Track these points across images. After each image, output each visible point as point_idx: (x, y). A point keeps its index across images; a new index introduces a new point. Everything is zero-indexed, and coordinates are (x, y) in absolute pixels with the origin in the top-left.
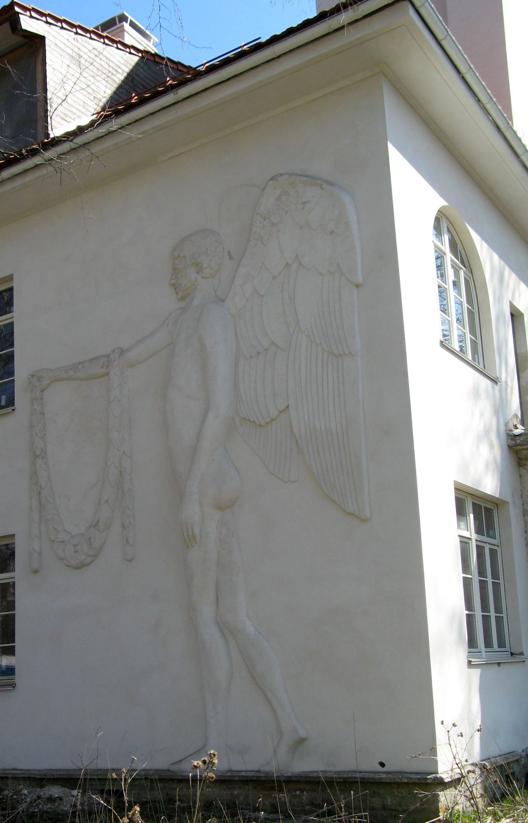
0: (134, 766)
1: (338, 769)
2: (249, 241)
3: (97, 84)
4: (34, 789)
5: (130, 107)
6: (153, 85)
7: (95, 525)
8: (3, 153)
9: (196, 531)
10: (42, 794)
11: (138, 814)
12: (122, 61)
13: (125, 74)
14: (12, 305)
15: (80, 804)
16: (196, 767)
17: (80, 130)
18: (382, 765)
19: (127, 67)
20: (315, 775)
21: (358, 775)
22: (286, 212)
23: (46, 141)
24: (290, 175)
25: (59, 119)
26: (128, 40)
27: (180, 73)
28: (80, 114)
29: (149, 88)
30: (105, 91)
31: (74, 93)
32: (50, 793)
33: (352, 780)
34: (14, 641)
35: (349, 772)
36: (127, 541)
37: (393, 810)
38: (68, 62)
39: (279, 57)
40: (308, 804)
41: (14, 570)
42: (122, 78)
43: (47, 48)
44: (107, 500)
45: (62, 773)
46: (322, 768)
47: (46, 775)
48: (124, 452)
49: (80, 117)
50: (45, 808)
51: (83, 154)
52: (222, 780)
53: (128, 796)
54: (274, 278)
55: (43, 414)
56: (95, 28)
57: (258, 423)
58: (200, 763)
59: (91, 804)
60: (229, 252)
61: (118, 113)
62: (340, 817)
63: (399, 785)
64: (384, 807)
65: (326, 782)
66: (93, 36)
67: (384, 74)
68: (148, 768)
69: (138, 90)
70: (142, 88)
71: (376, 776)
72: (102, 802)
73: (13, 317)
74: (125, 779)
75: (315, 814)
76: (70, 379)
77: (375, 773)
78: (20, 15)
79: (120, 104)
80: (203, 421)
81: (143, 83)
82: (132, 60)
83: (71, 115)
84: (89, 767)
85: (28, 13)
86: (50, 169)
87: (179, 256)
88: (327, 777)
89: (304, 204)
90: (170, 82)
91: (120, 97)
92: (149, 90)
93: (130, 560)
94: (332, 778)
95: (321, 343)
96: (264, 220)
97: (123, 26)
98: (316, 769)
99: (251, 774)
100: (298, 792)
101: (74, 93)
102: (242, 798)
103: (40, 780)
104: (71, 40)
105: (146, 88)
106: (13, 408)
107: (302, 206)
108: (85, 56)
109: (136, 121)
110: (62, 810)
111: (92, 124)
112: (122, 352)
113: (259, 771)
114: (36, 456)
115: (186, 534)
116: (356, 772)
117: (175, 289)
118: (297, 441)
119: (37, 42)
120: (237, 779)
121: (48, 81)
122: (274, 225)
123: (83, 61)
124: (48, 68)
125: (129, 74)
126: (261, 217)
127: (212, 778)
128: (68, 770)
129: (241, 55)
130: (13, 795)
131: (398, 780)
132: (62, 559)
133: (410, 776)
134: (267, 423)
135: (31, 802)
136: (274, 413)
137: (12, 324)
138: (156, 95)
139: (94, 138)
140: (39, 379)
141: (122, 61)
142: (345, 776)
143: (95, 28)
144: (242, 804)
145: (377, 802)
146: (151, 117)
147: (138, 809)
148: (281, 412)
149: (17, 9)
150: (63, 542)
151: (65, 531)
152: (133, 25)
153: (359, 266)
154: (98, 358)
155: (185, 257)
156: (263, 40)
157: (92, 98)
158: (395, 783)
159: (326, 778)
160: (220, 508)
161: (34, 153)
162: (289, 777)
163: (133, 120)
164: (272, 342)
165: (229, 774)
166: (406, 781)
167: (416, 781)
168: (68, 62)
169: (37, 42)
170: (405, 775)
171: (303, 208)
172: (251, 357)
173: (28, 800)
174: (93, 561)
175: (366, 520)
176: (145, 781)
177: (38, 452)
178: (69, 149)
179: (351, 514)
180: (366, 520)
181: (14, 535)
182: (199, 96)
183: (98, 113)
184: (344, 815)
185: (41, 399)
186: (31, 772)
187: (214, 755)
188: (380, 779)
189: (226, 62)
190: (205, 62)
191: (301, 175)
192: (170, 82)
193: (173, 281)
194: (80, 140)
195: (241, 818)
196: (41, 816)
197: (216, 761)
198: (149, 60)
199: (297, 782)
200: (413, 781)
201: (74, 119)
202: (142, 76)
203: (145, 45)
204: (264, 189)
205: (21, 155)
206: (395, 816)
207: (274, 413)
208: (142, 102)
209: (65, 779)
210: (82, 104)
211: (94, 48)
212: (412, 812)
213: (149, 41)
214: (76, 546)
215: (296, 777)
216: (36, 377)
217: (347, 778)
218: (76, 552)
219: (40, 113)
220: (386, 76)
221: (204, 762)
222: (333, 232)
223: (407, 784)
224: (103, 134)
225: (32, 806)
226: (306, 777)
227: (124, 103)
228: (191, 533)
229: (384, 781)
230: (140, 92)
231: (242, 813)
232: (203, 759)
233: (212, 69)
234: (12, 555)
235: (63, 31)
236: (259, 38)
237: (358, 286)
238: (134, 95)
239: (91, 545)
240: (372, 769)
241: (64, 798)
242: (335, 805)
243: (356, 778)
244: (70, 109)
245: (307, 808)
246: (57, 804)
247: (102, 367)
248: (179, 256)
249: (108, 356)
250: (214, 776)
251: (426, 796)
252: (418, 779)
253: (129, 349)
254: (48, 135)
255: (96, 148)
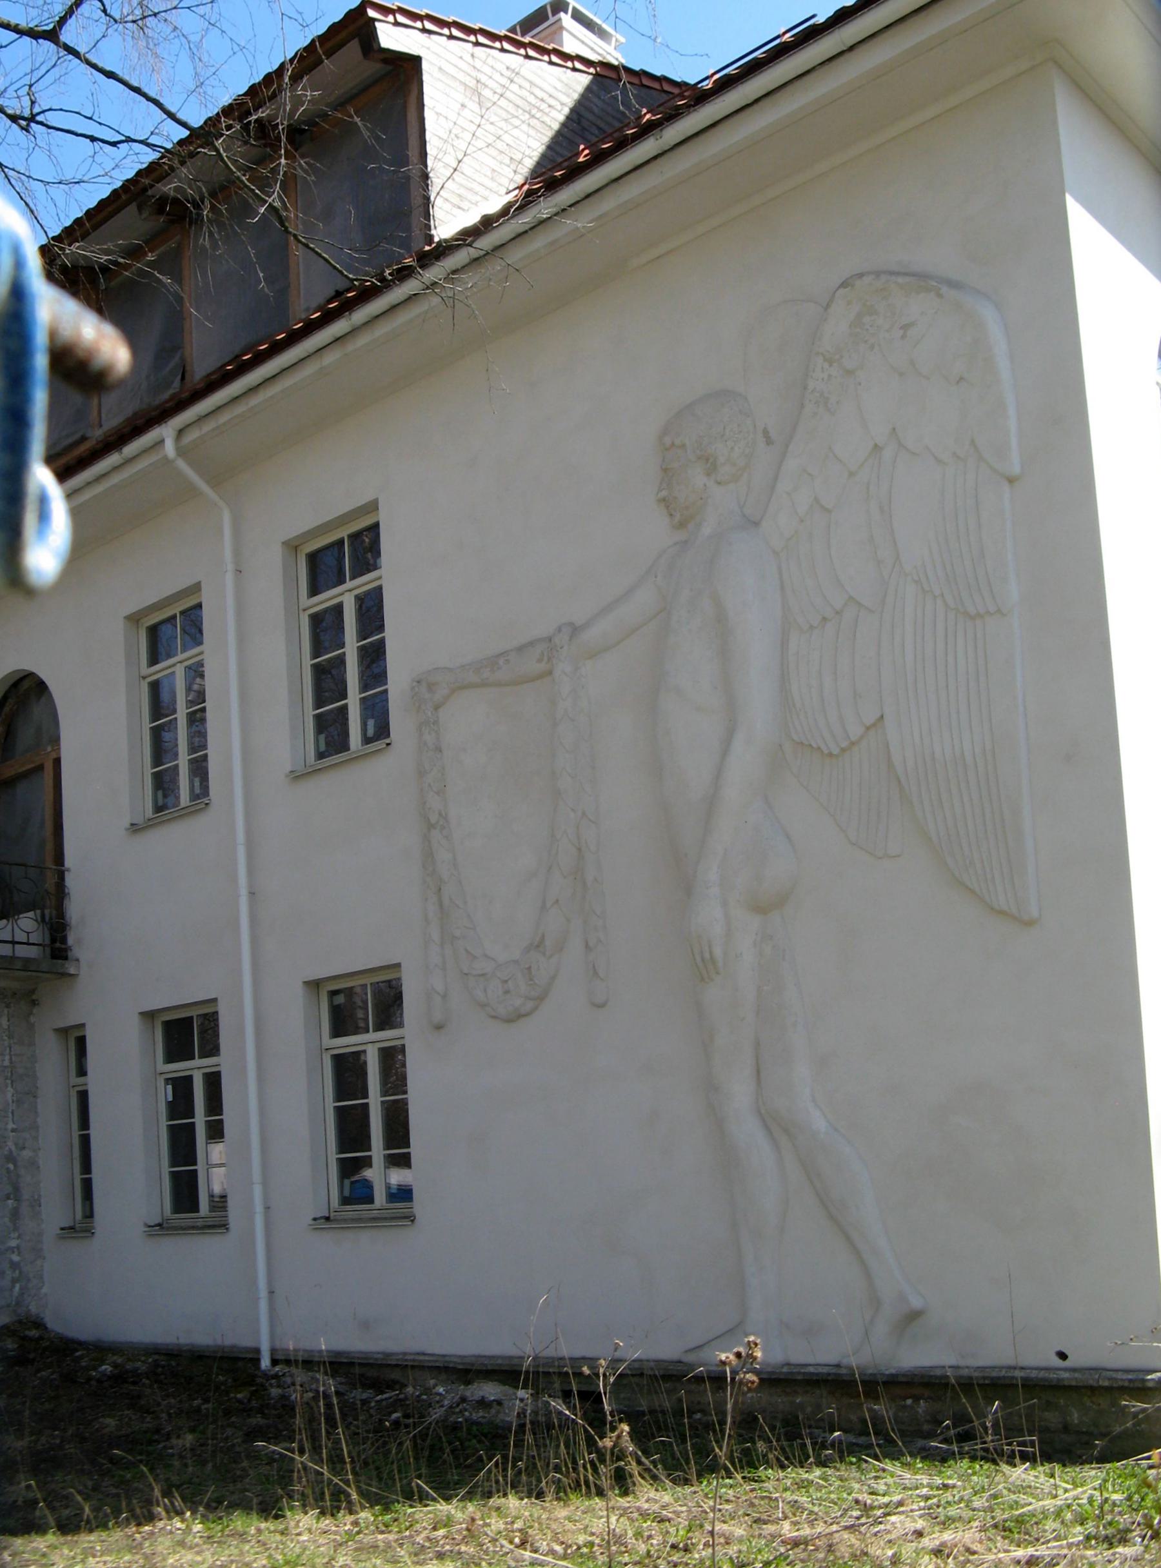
0: (618, 1354)
1: (981, 1363)
2: (802, 406)
3: (516, 132)
4: (454, 1386)
5: (576, 172)
6: (617, 125)
7: (538, 946)
8: (352, 280)
9: (718, 952)
10: (468, 1394)
11: (626, 1437)
12: (559, 86)
13: (566, 111)
14: (378, 554)
15: (532, 1411)
16: (723, 1363)
17: (488, 223)
18: (1063, 1356)
19: (568, 96)
20: (938, 1372)
21: (1018, 1374)
22: (872, 347)
23: (427, 248)
24: (878, 274)
25: (447, 206)
26: (570, 46)
27: (665, 97)
28: (486, 193)
29: (610, 131)
30: (531, 145)
31: (474, 155)
32: (481, 1393)
33: (1007, 1382)
34: (408, 1146)
35: (1001, 1368)
36: (596, 973)
37: (1083, 1433)
38: (461, 98)
39: (851, 48)
40: (928, 1422)
41: (401, 1025)
42: (561, 118)
43: (426, 77)
44: (557, 901)
45: (500, 1361)
46: (952, 1361)
47: (473, 1365)
48: (584, 814)
49: (486, 199)
50: (475, 1416)
51: (495, 266)
52: (775, 1380)
53: (610, 1405)
54: (852, 474)
55: (439, 749)
56: (509, 31)
57: (826, 752)
58: (732, 1357)
59: (548, 1413)
60: (766, 432)
61: (552, 185)
62: (985, 1443)
63: (1093, 1390)
64: (1066, 1428)
65: (960, 1385)
66: (506, 46)
67: (1056, 62)
68: (644, 1357)
69: (590, 137)
70: (596, 132)
71: (1052, 1376)
72: (567, 1412)
73: (380, 578)
74: (604, 1375)
75: (941, 1438)
76: (484, 684)
77: (1047, 1369)
78: (377, 24)
79: (558, 166)
80: (725, 753)
81: (599, 122)
82: (579, 82)
83: (470, 196)
84: (545, 1354)
85: (391, 18)
86: (435, 300)
87: (673, 444)
88: (961, 1377)
89: (905, 327)
90: (648, 116)
91: (557, 153)
92: (611, 134)
93: (602, 1006)
94: (971, 1378)
95: (942, 595)
96: (831, 366)
97: (560, 19)
98: (942, 1363)
99: (825, 1370)
100: (909, 1402)
101: (474, 155)
102: (809, 1409)
103: (465, 1372)
104: (468, 58)
105: (605, 132)
106: (388, 741)
107: (901, 332)
108: (490, 83)
109: (588, 196)
110: (502, 1421)
111: (505, 211)
112: (575, 630)
113: (838, 1366)
114: (431, 827)
115: (698, 958)
116: (1015, 1368)
117: (667, 507)
118: (899, 782)
119: (407, 68)
120: (800, 1377)
121: (427, 138)
122: (850, 373)
123: (487, 93)
124: (428, 114)
125: (573, 110)
126: (825, 360)
127: (753, 1382)
128: (511, 1358)
129: (780, 51)
130: (421, 1394)
131: (1091, 1382)
132: (483, 1006)
133: (1114, 1375)
134: (843, 750)
135: (451, 1407)
136: (855, 731)
137: (379, 589)
138: (622, 144)
139: (513, 235)
140: (431, 687)
141: (559, 86)
142: (994, 1374)
143: (509, 31)
144: (808, 1419)
145: (1052, 1418)
146: (615, 185)
147: (626, 1428)
148: (868, 728)
149: (371, 13)
150: (483, 975)
151: (486, 956)
152: (578, 17)
153: (1014, 442)
154: (531, 644)
155: (683, 446)
156: (820, 19)
157: (507, 161)
158: (1086, 1387)
159: (958, 1378)
160: (761, 908)
161: (404, 274)
162: (892, 1375)
163: (583, 196)
164: (851, 598)
165: (785, 1370)
166: (1106, 1384)
167: (1126, 1384)
168: (461, 98)
169: (407, 68)
170: (1104, 1373)
171: (903, 337)
172: (812, 627)
173: (446, 1403)
174: (536, 1008)
175: (1030, 923)
176: (641, 1379)
177: (433, 819)
178: (467, 261)
179: (1001, 912)
180: (1030, 923)
181: (398, 965)
182: (703, 137)
183: (520, 187)
184: (993, 1441)
185: (436, 723)
186: (447, 1359)
187: (756, 1344)
188: (1058, 1380)
189: (752, 68)
190: (712, 71)
191: (897, 274)
192: (648, 116)
193: (664, 493)
194: (485, 242)
195: (808, 1442)
196: (469, 1430)
197: (758, 1354)
198: (607, 75)
199: (907, 1383)
200: (1120, 1383)
201: (476, 204)
202: (596, 110)
203: (601, 51)
204: (828, 306)
205: (383, 280)
206: (1087, 1443)
207: (855, 731)
208: (599, 158)
209: (505, 1372)
210: (489, 173)
211: (508, 68)
212: (1119, 1436)
213: (609, 43)
214: (506, 981)
215: (904, 1375)
216: (424, 683)
217: (999, 1378)
218: (507, 992)
219: (417, 201)
220: (1060, 67)
221: (738, 1355)
222: (961, 379)
223: (1109, 1389)
224: (527, 227)
225: (454, 1413)
226: (922, 1376)
227: (566, 164)
228: (707, 956)
229: (1066, 1383)
230: (595, 139)
231: (810, 1434)
232: (735, 1350)
233: (726, 83)
234: (399, 997)
235: (453, 42)
236: (813, 16)
237: (1011, 480)
238: (582, 147)
239: (531, 980)
240: (1043, 1364)
241: (506, 1403)
242: (976, 1423)
243: (1013, 1378)
244: (469, 185)
245: (926, 1427)
246: (493, 1411)
247: (540, 661)
248: (673, 444)
249: (550, 639)
250: (755, 1378)
251: (1144, 1410)
252: (1130, 1381)
253: (587, 625)
254: (431, 237)
255: (515, 255)
